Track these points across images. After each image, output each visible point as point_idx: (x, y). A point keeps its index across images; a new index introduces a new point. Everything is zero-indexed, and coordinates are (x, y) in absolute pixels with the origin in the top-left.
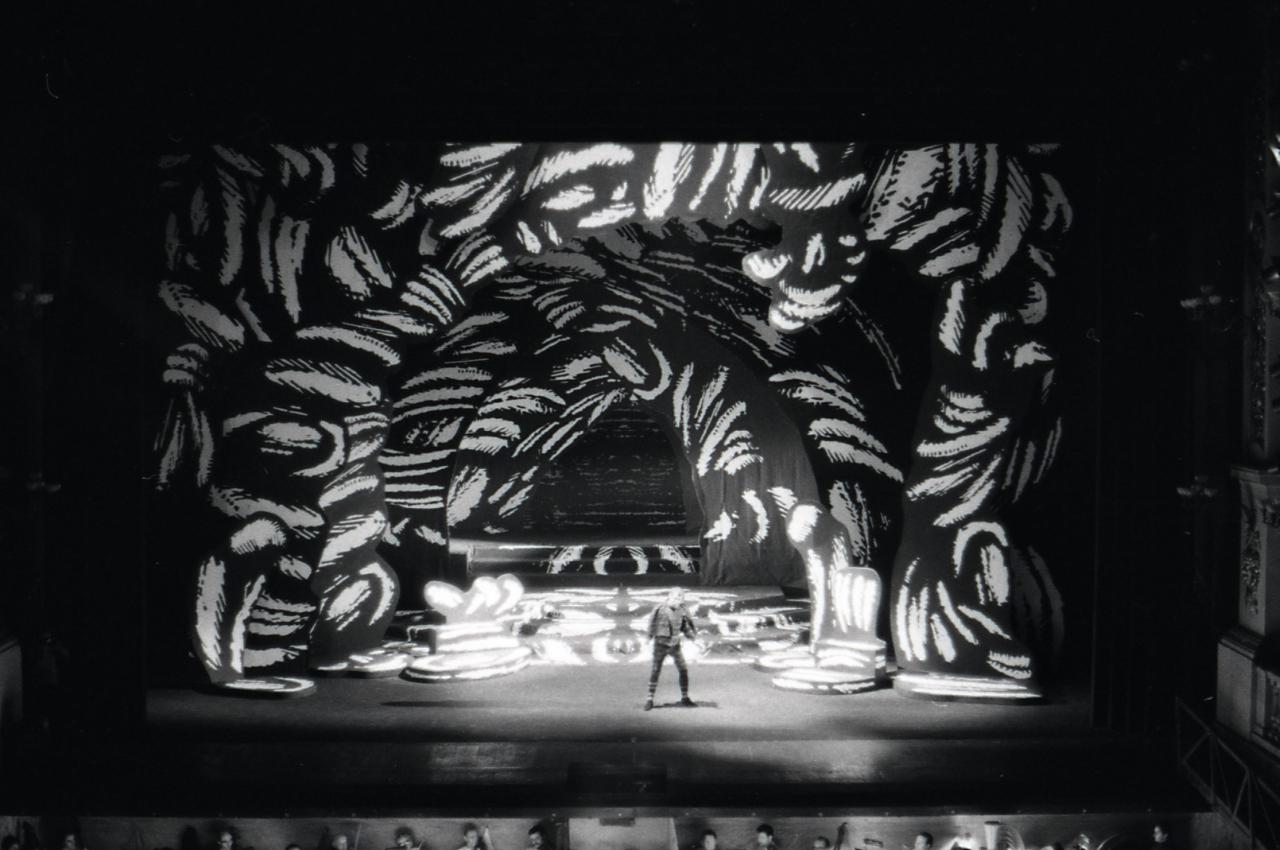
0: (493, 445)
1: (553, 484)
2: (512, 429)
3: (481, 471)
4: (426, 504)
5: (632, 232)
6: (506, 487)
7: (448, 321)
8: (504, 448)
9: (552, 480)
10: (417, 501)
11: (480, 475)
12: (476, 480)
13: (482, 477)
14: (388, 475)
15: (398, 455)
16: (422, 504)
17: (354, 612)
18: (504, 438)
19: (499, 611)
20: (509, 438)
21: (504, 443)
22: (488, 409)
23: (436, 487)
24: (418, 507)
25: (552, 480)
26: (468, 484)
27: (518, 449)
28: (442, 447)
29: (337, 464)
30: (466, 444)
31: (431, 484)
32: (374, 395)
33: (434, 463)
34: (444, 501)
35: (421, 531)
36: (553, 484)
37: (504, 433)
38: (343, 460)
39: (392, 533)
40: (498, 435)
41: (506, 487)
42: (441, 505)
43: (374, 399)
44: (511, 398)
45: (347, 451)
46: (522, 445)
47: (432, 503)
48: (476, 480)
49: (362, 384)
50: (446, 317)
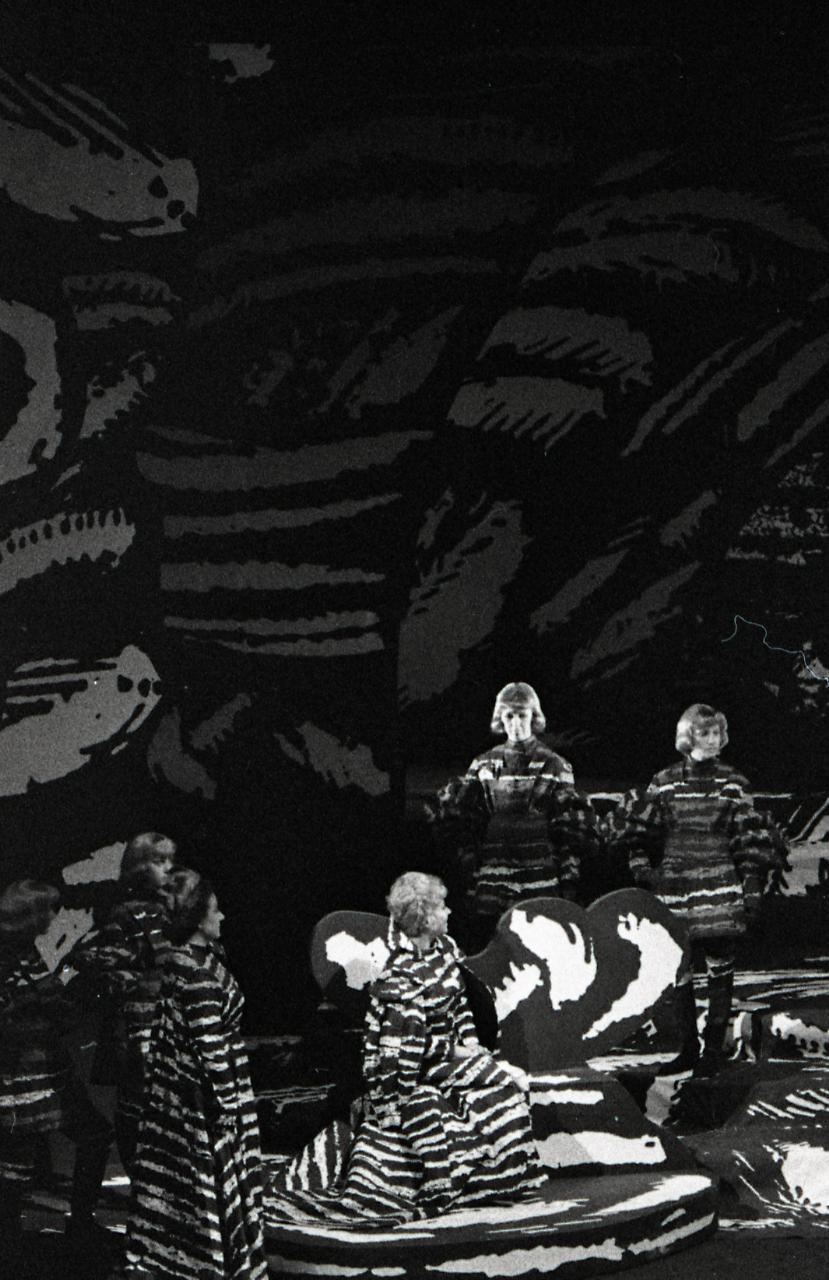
0: (549, 406)
1: (797, 559)
2: (629, 351)
3: (500, 509)
4: (317, 638)
5: (56, 670)
6: (601, 569)
7: (170, 307)
8: (590, 417)
9: (794, 545)
10: (286, 627)
11: (499, 522)
12: (482, 544)
13: (503, 538)
14: (176, 526)
15: (214, 451)
16: (307, 640)
17: (752, 1001)
18: (590, 383)
19: (790, 1109)
20: (609, 384)
21: (592, 401)
22: (544, 265)
23: (354, 576)
24: (287, 649)
25: (794, 545)
26: (451, 557)
27: (646, 424)
28: (376, 421)
29: (35, 456)
30: (468, 408)
31: (336, 565)
32: (175, 195)
33: (351, 484)
34: (388, 629)
35: (299, 742)
36: (797, 559)
37: (592, 363)
38: (55, 439)
39: (187, 746)
40: (570, 369)
41: (601, 569)
42: (372, 643)
43: (176, 208)
44: (619, 228)
45: (71, 406)
46: (659, 409)
47: (338, 634)
48: (482, 544)
49: (129, 153)
50: (159, 302)
